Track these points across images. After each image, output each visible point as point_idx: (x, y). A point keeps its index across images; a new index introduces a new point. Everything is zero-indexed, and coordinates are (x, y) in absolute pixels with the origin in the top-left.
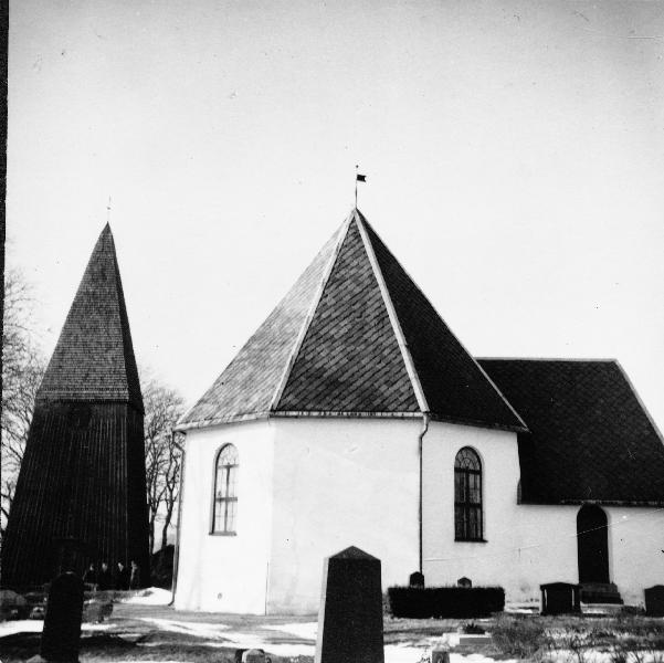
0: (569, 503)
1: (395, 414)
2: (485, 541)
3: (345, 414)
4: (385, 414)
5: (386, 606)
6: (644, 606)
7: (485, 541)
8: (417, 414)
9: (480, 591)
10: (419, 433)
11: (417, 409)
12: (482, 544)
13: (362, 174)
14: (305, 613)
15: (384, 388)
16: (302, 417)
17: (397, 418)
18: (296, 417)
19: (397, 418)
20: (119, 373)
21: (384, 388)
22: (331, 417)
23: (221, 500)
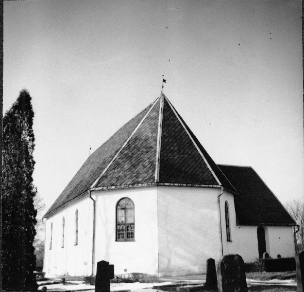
0: (255, 225)
1: (209, 186)
2: (232, 241)
3: (189, 185)
4: (205, 186)
5: (297, 261)
6: (246, 273)
7: (232, 241)
8: (218, 186)
9: (284, 259)
10: (219, 194)
11: (218, 184)
12: (230, 242)
13: (165, 79)
14: (185, 274)
15: (201, 174)
16: (171, 186)
17: (210, 187)
18: (169, 186)
19: (210, 187)
20: (143, 165)
21: (201, 174)
22: (183, 186)
23: (119, 225)
